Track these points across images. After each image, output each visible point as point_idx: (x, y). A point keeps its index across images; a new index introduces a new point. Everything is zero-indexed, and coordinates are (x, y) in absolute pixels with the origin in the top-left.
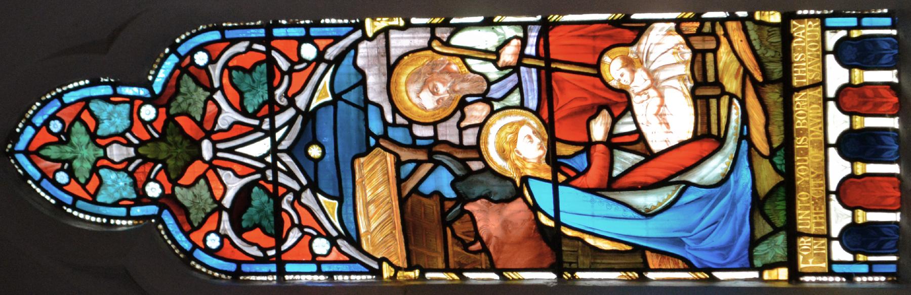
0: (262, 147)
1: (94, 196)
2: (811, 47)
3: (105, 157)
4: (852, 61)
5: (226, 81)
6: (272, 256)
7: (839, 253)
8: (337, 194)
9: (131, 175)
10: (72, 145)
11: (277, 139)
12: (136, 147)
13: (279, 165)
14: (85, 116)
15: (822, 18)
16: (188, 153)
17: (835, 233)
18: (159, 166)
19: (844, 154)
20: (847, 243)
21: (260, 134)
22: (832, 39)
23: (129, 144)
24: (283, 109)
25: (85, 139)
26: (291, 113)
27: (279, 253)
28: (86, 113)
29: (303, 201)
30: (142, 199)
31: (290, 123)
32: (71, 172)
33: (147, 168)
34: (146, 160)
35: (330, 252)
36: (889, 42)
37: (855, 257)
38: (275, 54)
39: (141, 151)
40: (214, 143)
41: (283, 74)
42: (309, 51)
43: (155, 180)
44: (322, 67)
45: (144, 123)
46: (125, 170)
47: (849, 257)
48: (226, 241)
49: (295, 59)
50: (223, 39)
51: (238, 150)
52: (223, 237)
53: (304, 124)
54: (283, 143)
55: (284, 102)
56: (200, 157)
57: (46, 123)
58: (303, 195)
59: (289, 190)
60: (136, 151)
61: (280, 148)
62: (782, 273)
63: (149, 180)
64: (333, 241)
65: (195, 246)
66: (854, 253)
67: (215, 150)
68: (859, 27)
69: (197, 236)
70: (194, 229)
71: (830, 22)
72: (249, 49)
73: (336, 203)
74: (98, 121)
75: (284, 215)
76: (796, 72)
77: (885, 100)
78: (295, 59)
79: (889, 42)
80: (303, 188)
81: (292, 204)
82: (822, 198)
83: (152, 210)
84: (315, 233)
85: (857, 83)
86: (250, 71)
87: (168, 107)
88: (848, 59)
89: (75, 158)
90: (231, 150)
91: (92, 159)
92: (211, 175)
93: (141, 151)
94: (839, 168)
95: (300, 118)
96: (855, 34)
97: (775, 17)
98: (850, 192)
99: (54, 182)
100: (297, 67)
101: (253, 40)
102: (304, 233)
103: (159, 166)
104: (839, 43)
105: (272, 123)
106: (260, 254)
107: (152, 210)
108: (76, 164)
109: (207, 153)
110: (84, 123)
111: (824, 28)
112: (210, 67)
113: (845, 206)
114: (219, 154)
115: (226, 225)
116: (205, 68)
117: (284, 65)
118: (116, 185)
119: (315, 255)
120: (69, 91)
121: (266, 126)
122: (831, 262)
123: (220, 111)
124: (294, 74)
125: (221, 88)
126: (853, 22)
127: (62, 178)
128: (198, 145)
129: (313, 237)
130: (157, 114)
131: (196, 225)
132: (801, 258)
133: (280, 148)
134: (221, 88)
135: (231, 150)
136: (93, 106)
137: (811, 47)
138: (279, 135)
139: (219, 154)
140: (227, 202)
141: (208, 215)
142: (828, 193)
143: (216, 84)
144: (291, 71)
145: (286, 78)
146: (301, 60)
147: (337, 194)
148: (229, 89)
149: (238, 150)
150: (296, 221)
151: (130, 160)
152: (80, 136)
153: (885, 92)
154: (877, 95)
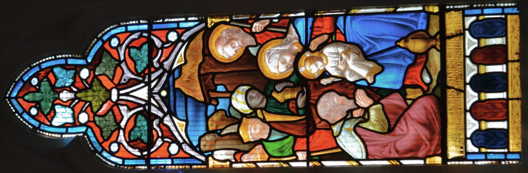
0: (143, 93)
1: (50, 122)
2: (458, 65)
3: (58, 98)
4: (481, 116)
5: (127, 56)
6: (145, 155)
7: (471, 148)
8: (185, 118)
9: (73, 109)
10: (42, 100)
11: (152, 87)
12: (76, 93)
13: (153, 101)
14: (51, 76)
15: (463, 10)
16: (104, 97)
17: (469, 135)
18: (88, 103)
19: (474, 90)
20: (475, 32)
21: (143, 84)
22: (469, 21)
23: (71, 91)
24: (157, 70)
25: (49, 88)
26: (161, 71)
27: (149, 153)
28: (51, 74)
29: (165, 122)
30: (76, 123)
31: (160, 77)
32: (39, 109)
33: (82, 104)
34: (80, 100)
35: (178, 152)
36: (502, 103)
37: (479, 150)
38: (153, 37)
39: (79, 95)
40: (118, 90)
41: (158, 49)
42: (173, 37)
43: (85, 111)
44: (180, 44)
45: (82, 80)
46: (69, 106)
47: (476, 150)
48: (122, 148)
49: (164, 40)
50: (127, 31)
51: (131, 94)
52: (120, 144)
53: (168, 77)
54: (156, 89)
55: (157, 65)
56: (110, 99)
57: (33, 117)
58: (165, 119)
59: (156, 117)
60: (75, 95)
61: (153, 92)
62: (438, 160)
63: (81, 111)
64: (180, 145)
65: (104, 149)
66: (479, 147)
67: (119, 95)
68: (483, 14)
69: (106, 145)
70: (105, 140)
71: (467, 12)
72: (141, 36)
73: (184, 123)
74: (56, 79)
75: (154, 133)
76: (449, 46)
77: (498, 82)
78: (164, 40)
79: (502, 103)
80: (165, 115)
81: (159, 125)
82: (461, 74)
83: (83, 129)
84: (170, 141)
85: (483, 129)
86: (139, 48)
87: (94, 71)
88: (477, 33)
89: (42, 100)
90: (127, 94)
91: (52, 100)
92: (115, 108)
93: (79, 95)
94: (472, 96)
95: (166, 74)
96: (481, 18)
97: (436, 9)
98: (480, 111)
99: (29, 114)
100: (166, 46)
101: (142, 31)
102: (164, 142)
103: (88, 103)
104: (473, 52)
105: (150, 78)
106: (139, 154)
107: (83, 129)
108: (43, 104)
109: (114, 98)
110: (49, 81)
111: (464, 16)
112: (119, 48)
113: (475, 119)
114: (121, 97)
115: (121, 138)
116: (116, 48)
117: (158, 43)
118: (63, 116)
119: (170, 155)
120: (43, 62)
121: (146, 80)
122: (467, 153)
123: (123, 73)
124: (164, 50)
125: (125, 60)
126: (479, 12)
127: (34, 111)
128: (109, 91)
129: (170, 144)
130: (90, 74)
131: (106, 138)
132: (448, 110)
133: (153, 92)
134: (125, 60)
135: (127, 94)
136: (56, 70)
137: (458, 65)
138: (153, 84)
139: (121, 97)
140: (123, 124)
141: (113, 132)
142: (466, 138)
143: (122, 58)
144: (162, 48)
145: (160, 51)
146: (168, 41)
147: (185, 118)
148: (129, 61)
149: (131, 94)
150: (160, 134)
151: (72, 100)
152: (45, 86)
153: (498, 24)
154: (494, 107)
